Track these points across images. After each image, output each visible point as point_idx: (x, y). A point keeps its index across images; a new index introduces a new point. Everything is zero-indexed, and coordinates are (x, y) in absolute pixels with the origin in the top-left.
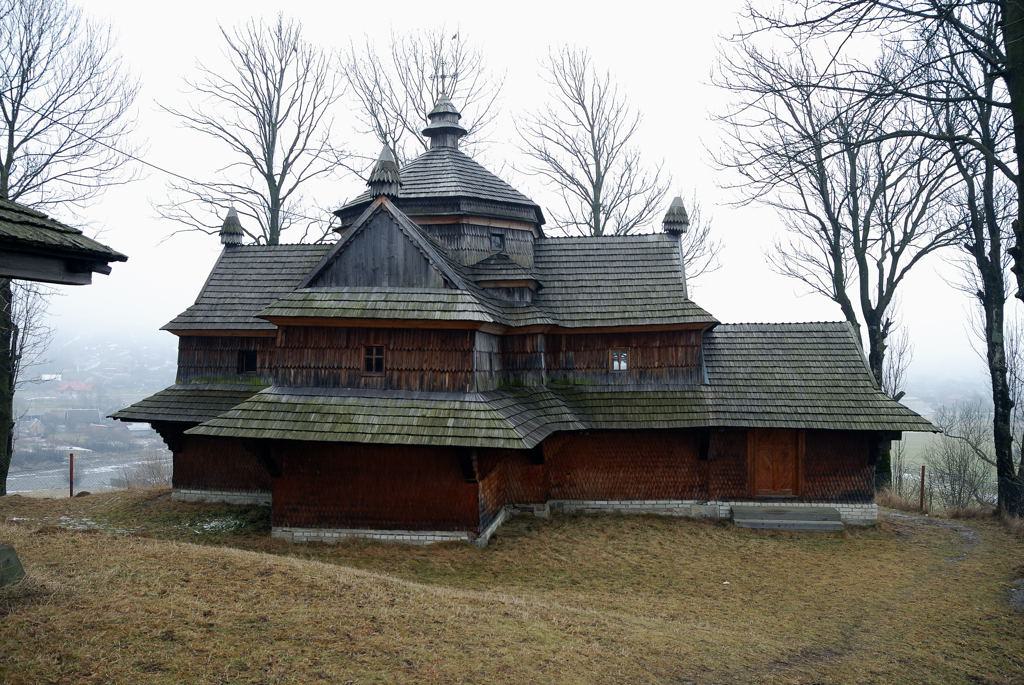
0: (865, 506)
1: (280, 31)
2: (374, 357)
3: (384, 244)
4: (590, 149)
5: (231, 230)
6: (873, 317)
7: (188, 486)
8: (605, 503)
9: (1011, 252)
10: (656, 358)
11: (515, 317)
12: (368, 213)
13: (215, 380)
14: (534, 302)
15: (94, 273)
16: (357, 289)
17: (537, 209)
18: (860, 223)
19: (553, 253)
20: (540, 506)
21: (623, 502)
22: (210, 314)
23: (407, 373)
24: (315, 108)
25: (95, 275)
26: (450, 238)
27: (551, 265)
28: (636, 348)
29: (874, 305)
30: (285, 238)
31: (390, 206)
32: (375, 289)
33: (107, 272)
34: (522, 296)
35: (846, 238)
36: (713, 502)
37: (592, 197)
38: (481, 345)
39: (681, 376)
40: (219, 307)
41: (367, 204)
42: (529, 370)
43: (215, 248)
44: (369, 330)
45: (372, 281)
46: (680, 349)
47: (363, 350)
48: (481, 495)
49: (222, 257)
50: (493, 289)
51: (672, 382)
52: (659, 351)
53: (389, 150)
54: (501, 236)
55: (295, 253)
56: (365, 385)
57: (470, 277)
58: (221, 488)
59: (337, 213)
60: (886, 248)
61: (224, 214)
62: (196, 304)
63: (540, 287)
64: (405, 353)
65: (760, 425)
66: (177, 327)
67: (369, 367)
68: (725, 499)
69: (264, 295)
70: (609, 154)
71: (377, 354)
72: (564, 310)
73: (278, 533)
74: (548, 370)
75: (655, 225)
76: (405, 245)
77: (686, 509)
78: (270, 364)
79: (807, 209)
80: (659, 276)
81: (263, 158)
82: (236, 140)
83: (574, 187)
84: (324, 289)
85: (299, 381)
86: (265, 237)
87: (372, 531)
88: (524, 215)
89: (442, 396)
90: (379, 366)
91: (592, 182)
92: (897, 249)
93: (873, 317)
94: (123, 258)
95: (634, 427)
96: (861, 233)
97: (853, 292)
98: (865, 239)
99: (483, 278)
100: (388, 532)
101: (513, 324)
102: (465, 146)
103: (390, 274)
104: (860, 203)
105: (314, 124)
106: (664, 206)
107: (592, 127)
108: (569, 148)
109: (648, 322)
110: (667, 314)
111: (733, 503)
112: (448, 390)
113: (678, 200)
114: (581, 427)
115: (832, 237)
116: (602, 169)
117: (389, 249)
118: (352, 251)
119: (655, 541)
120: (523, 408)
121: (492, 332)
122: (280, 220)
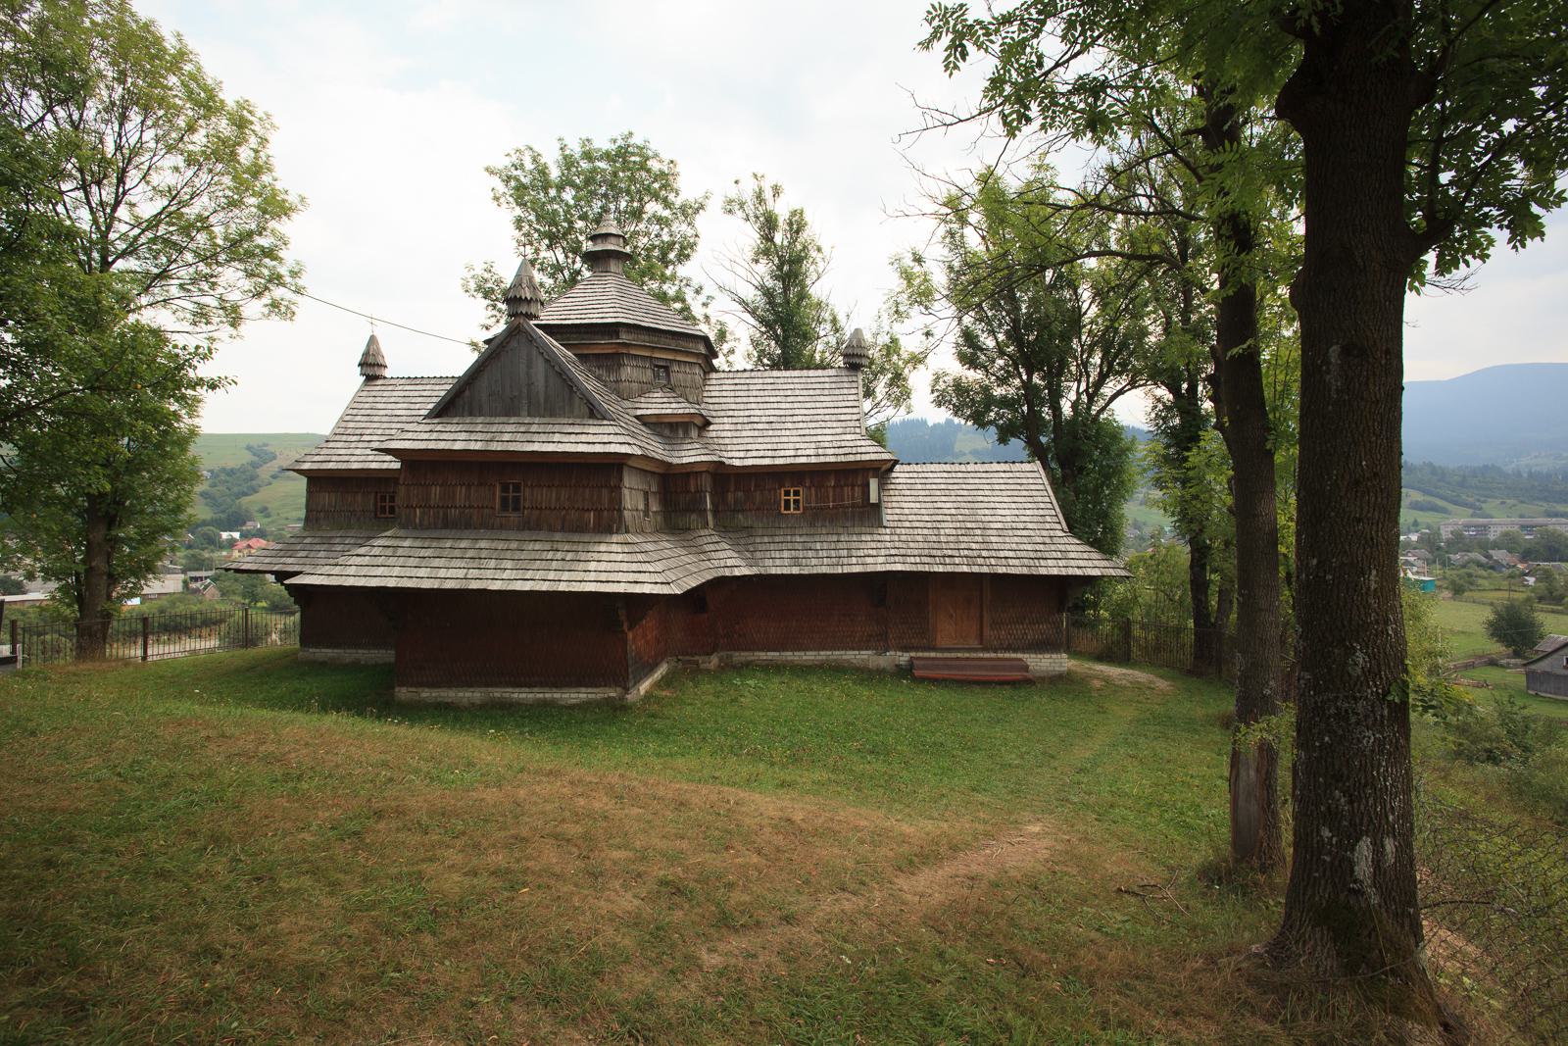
0: (1054, 656)
2: (511, 495)
7: (318, 644)
9: (1210, 379)
20: (706, 658)
23: (548, 512)
26: (609, 370)
32: (513, 420)
36: (893, 653)
38: (630, 481)
42: (693, 511)
54: (666, 368)
60: (1081, 390)
65: (941, 569)
68: (905, 649)
76: (546, 371)
77: (863, 660)
87: (510, 690)
88: (692, 347)
90: (516, 509)
100: (527, 690)
110: (841, 451)
111: (913, 654)
114: (746, 571)
119: (775, 685)
121: (648, 468)
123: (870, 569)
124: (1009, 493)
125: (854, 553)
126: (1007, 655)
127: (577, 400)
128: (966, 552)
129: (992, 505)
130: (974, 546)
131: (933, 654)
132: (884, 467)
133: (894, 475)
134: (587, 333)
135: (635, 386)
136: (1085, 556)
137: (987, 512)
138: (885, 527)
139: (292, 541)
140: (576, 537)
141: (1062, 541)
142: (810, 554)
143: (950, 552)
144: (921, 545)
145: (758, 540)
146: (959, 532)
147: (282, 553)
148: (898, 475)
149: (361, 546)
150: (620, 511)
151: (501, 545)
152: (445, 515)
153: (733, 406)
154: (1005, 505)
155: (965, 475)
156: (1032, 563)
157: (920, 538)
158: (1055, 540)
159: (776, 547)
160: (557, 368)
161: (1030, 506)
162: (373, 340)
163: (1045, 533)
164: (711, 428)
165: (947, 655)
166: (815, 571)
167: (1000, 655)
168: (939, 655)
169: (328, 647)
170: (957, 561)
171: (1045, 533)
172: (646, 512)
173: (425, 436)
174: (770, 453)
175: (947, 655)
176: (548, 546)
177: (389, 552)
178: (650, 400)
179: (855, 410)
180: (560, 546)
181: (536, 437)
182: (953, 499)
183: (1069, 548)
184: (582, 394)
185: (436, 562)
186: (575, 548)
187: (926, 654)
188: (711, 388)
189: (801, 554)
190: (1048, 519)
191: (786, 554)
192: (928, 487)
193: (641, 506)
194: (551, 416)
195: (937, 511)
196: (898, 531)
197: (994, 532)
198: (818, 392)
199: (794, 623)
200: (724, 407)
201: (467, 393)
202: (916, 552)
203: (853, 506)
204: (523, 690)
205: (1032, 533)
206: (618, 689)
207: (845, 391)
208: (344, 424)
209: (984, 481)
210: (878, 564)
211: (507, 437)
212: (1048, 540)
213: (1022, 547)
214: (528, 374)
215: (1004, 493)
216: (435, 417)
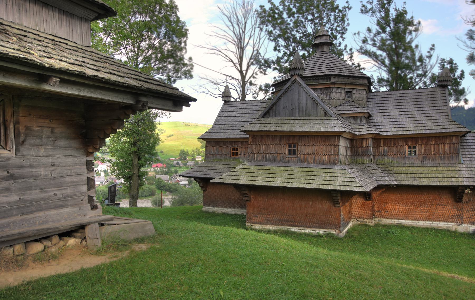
1: (244, 4)
3: (297, 97)
5: (226, 96)
7: (209, 205)
8: (404, 221)
10: (433, 150)
11: (357, 130)
12: (289, 83)
13: (221, 160)
14: (367, 122)
15: (183, 107)
16: (284, 118)
19: (377, 99)
21: (413, 221)
22: (218, 131)
23: (307, 156)
24: (260, 39)
26: (326, 94)
27: (375, 105)
28: (421, 145)
30: (249, 98)
31: (299, 79)
32: (293, 118)
33: (189, 106)
34: (361, 120)
36: (466, 225)
39: (446, 159)
40: (222, 128)
41: (289, 80)
43: (220, 102)
44: (290, 136)
46: (446, 145)
47: (287, 145)
48: (342, 213)
49: (223, 107)
51: (442, 162)
52: (434, 147)
55: (255, 104)
56: (288, 161)
58: (223, 207)
61: (223, 89)
63: (370, 116)
64: (306, 147)
66: (206, 137)
67: (290, 153)
69: (241, 123)
71: (293, 147)
72: (382, 127)
73: (248, 225)
77: (449, 227)
78: (244, 153)
80: (434, 108)
81: (238, 63)
82: (227, 56)
84: (269, 119)
85: (259, 159)
86: (239, 98)
89: (324, 166)
90: (294, 153)
94: (195, 100)
95: (420, 184)
99: (342, 112)
100: (298, 228)
101: (358, 133)
103: (299, 111)
105: (260, 46)
109: (428, 132)
112: (327, 164)
118: (281, 102)
120: (361, 173)
121: (347, 137)
122: (246, 90)
125: (409, 175)
127: (319, 109)
132: (462, 135)
133: (466, 138)
134: (317, 79)
139: (202, 165)
147: (198, 170)
149: (235, 168)
152: (266, 156)
153: (382, 108)
164: (371, 118)
169: (208, 206)
172: (346, 156)
174: (401, 129)
178: (344, 107)
179: (445, 108)
188: (370, 100)
193: (345, 154)
198: (424, 100)
199: (413, 208)
200: (377, 108)
201: (274, 108)
206: (337, 231)
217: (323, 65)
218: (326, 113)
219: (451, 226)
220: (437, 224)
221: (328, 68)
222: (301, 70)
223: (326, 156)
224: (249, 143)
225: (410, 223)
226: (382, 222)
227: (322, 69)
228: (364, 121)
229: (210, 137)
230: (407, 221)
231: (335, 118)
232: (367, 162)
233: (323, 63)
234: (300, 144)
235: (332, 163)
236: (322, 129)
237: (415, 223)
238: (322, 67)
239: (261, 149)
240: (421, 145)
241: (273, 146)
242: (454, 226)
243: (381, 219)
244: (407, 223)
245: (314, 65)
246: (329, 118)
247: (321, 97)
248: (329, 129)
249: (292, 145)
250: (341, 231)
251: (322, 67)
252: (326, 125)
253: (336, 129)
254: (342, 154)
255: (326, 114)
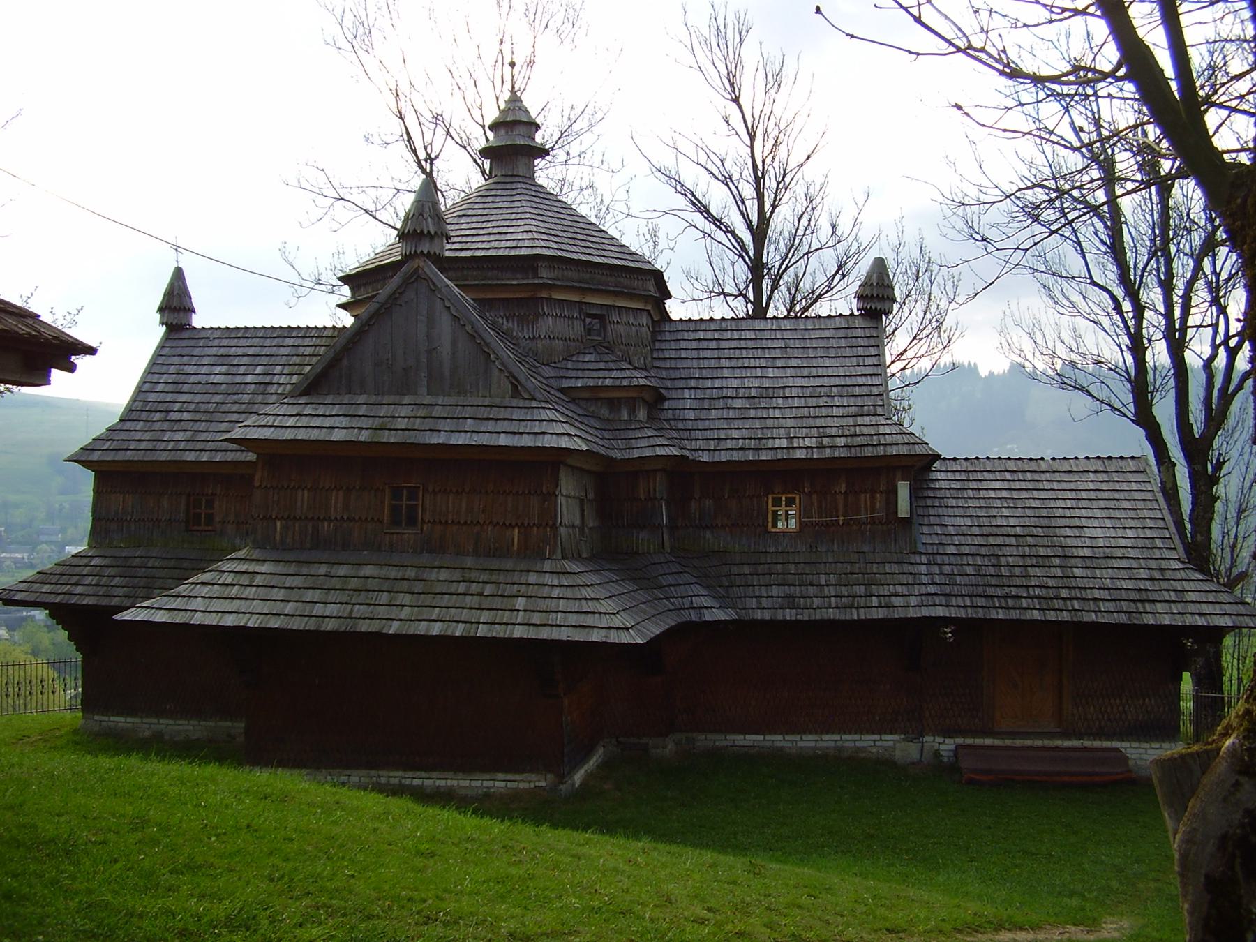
4: (748, 173)
6: (1196, 449)
7: (107, 709)
17: (658, 276)
18: (1175, 298)
25: (55, 374)
29: (1197, 428)
31: (432, 270)
32: (406, 400)
33: (71, 368)
34: (632, 412)
35: (1153, 320)
37: (751, 253)
38: (568, 486)
45: (403, 385)
49: (161, 347)
50: (587, 400)
53: (430, 187)
54: (601, 318)
57: (553, 382)
59: (346, 279)
60: (1218, 341)
62: (121, 421)
66: (95, 456)
67: (395, 522)
68: (948, 733)
70: (778, 183)
71: (409, 498)
74: (672, 528)
75: (842, 303)
77: (886, 748)
79: (1091, 277)
83: (720, 235)
84: (329, 400)
90: (412, 521)
91: (750, 226)
92: (1233, 342)
93: (1196, 449)
94: (91, 351)
96: (1177, 312)
97: (1164, 410)
98: (1184, 327)
99: (572, 383)
100: (423, 774)
102: (546, 174)
104: (1177, 266)
106: (860, 271)
107: (752, 137)
108: (716, 172)
111: (959, 741)
113: (880, 264)
114: (720, 615)
115: (1131, 323)
116: (767, 207)
117: (428, 336)
120: (630, 587)
121: (586, 467)
123: (897, 614)
124: (1102, 504)
126: (1097, 744)
127: (496, 373)
128: (1037, 591)
129: (1077, 522)
130: (1051, 583)
131: (988, 741)
135: (559, 344)
136: (1211, 598)
137: (1069, 532)
138: (921, 553)
140: (495, 564)
141: (1179, 575)
142: (812, 590)
143: (1014, 591)
144: (973, 580)
145: (735, 570)
146: (1029, 561)
148: (939, 476)
149: (203, 570)
150: (554, 527)
151: (393, 573)
154: (1096, 523)
155: (1037, 477)
156: (1132, 607)
157: (970, 570)
158: (1168, 574)
159: (762, 580)
160: (469, 328)
161: (1131, 523)
162: (179, 274)
163: (1153, 564)
164: (666, 405)
165: (1008, 742)
166: (818, 616)
167: (1087, 743)
168: (997, 742)
169: (118, 714)
170: (1024, 603)
171: (1153, 564)
172: (582, 528)
173: (291, 421)
175: (1008, 742)
176: (457, 575)
177: (245, 580)
178: (580, 366)
180: (474, 575)
181: (442, 425)
182: (1019, 512)
183: (1187, 586)
184: (503, 364)
185: (310, 595)
186: (494, 578)
187: (979, 741)
189: (797, 591)
190: (1159, 543)
191: (776, 591)
192: (983, 494)
193: (578, 522)
194: (459, 394)
195: (995, 530)
196: (939, 559)
197: (1079, 562)
198: (820, 352)
201: (345, 362)
202: (965, 590)
203: (873, 521)
204: (418, 774)
205: (1134, 564)
207: (861, 351)
208: (142, 397)
209: (1065, 486)
210: (911, 606)
211: (401, 424)
212: (1157, 575)
213: (1119, 584)
214: (428, 336)
215: (1095, 504)
216: (301, 395)
217: (514, 223)
218: (515, 387)
219: (891, 743)
220: (855, 741)
221: (530, 236)
222: (436, 240)
223: (516, 530)
224: (257, 484)
225: (779, 744)
226: (698, 744)
227: (509, 237)
228: (642, 414)
229: (110, 457)
230: (768, 737)
231: (544, 405)
232: (649, 548)
233: (513, 216)
234: (430, 490)
235: (533, 552)
236: (503, 441)
237: (792, 741)
238: (511, 230)
239: (299, 504)
240: (810, 494)
241: (341, 493)
242: (898, 745)
243: (694, 735)
244: (768, 744)
245: (484, 219)
246: (527, 404)
247: (505, 327)
248: (526, 441)
249: (405, 492)
250: (561, 778)
251: (511, 230)
252: (514, 427)
253: (547, 441)
254: (566, 521)
255: (516, 393)
